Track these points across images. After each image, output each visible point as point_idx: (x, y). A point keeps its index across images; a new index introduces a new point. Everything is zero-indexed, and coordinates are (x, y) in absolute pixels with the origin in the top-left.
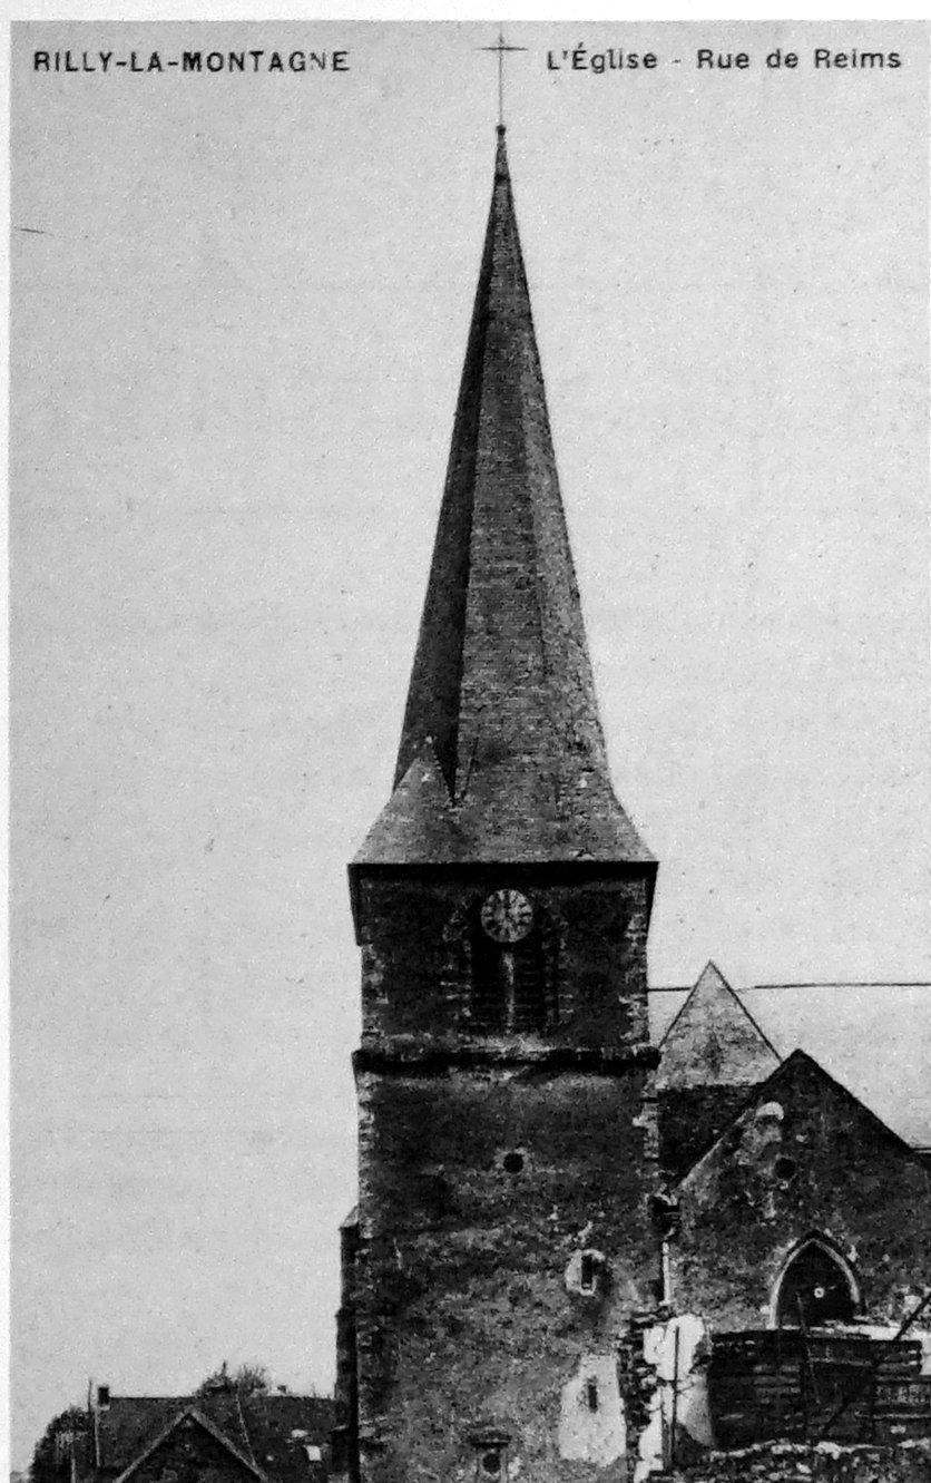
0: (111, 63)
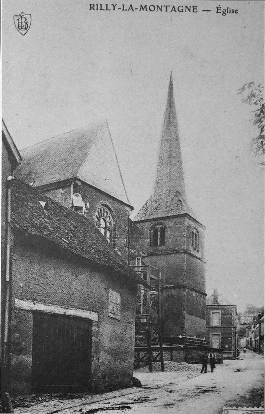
0: (116, 8)
